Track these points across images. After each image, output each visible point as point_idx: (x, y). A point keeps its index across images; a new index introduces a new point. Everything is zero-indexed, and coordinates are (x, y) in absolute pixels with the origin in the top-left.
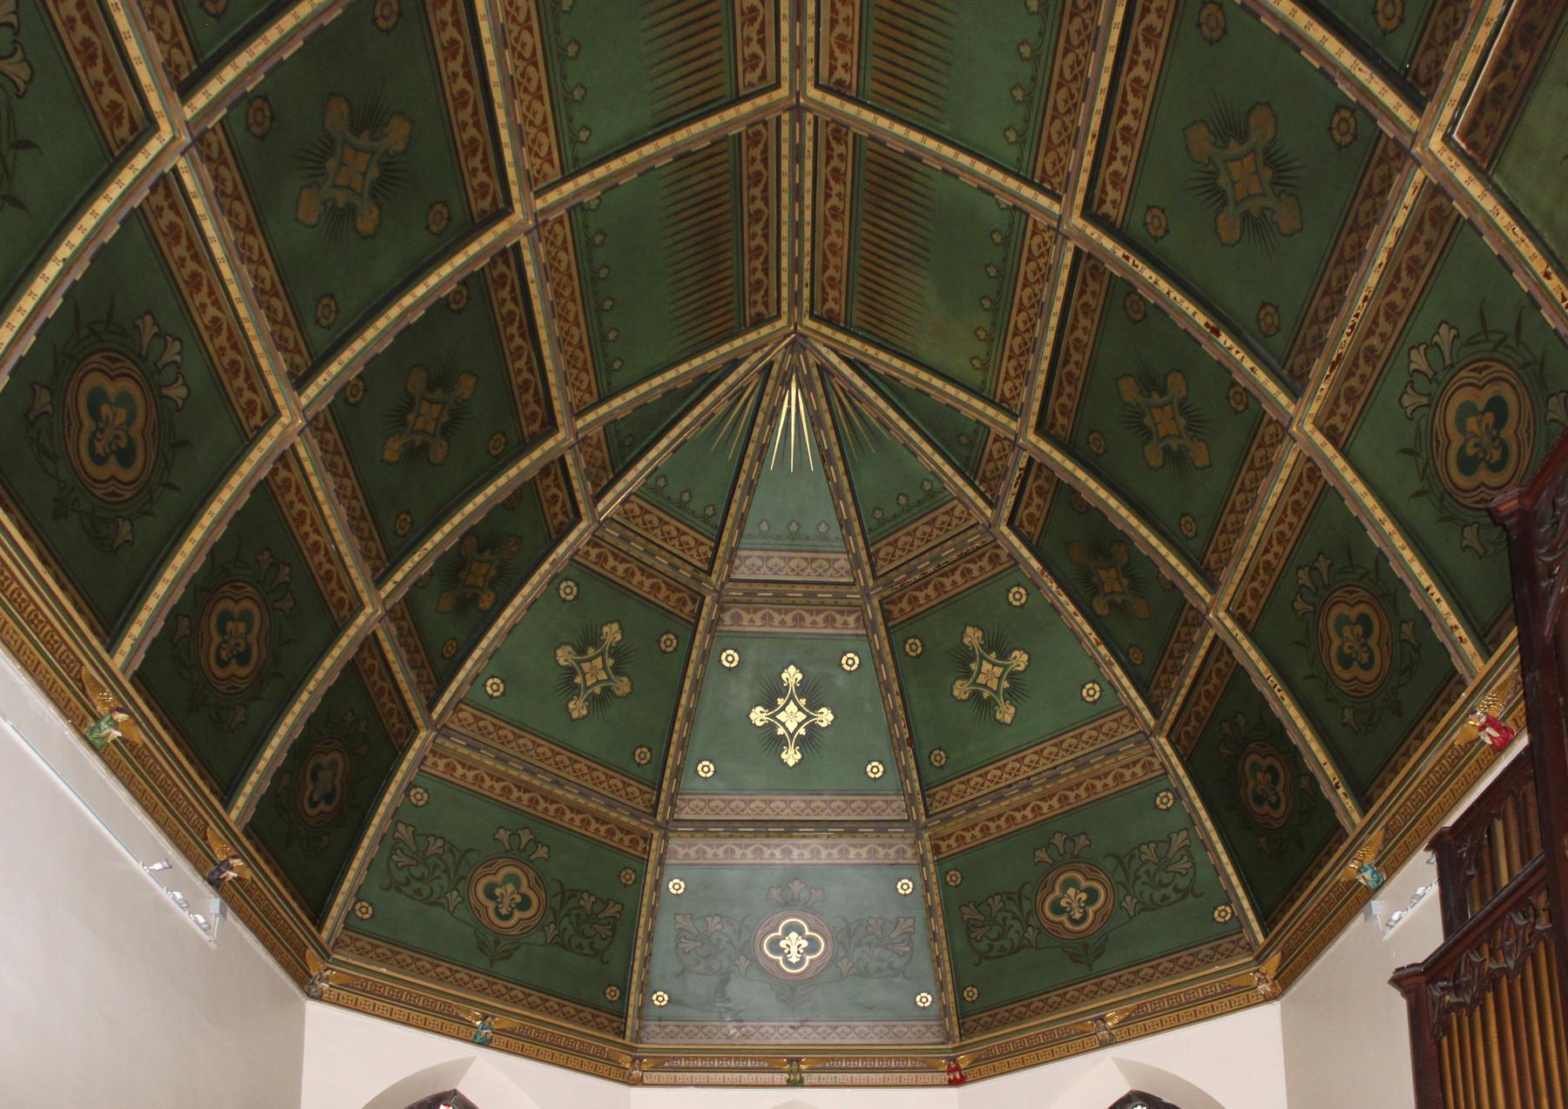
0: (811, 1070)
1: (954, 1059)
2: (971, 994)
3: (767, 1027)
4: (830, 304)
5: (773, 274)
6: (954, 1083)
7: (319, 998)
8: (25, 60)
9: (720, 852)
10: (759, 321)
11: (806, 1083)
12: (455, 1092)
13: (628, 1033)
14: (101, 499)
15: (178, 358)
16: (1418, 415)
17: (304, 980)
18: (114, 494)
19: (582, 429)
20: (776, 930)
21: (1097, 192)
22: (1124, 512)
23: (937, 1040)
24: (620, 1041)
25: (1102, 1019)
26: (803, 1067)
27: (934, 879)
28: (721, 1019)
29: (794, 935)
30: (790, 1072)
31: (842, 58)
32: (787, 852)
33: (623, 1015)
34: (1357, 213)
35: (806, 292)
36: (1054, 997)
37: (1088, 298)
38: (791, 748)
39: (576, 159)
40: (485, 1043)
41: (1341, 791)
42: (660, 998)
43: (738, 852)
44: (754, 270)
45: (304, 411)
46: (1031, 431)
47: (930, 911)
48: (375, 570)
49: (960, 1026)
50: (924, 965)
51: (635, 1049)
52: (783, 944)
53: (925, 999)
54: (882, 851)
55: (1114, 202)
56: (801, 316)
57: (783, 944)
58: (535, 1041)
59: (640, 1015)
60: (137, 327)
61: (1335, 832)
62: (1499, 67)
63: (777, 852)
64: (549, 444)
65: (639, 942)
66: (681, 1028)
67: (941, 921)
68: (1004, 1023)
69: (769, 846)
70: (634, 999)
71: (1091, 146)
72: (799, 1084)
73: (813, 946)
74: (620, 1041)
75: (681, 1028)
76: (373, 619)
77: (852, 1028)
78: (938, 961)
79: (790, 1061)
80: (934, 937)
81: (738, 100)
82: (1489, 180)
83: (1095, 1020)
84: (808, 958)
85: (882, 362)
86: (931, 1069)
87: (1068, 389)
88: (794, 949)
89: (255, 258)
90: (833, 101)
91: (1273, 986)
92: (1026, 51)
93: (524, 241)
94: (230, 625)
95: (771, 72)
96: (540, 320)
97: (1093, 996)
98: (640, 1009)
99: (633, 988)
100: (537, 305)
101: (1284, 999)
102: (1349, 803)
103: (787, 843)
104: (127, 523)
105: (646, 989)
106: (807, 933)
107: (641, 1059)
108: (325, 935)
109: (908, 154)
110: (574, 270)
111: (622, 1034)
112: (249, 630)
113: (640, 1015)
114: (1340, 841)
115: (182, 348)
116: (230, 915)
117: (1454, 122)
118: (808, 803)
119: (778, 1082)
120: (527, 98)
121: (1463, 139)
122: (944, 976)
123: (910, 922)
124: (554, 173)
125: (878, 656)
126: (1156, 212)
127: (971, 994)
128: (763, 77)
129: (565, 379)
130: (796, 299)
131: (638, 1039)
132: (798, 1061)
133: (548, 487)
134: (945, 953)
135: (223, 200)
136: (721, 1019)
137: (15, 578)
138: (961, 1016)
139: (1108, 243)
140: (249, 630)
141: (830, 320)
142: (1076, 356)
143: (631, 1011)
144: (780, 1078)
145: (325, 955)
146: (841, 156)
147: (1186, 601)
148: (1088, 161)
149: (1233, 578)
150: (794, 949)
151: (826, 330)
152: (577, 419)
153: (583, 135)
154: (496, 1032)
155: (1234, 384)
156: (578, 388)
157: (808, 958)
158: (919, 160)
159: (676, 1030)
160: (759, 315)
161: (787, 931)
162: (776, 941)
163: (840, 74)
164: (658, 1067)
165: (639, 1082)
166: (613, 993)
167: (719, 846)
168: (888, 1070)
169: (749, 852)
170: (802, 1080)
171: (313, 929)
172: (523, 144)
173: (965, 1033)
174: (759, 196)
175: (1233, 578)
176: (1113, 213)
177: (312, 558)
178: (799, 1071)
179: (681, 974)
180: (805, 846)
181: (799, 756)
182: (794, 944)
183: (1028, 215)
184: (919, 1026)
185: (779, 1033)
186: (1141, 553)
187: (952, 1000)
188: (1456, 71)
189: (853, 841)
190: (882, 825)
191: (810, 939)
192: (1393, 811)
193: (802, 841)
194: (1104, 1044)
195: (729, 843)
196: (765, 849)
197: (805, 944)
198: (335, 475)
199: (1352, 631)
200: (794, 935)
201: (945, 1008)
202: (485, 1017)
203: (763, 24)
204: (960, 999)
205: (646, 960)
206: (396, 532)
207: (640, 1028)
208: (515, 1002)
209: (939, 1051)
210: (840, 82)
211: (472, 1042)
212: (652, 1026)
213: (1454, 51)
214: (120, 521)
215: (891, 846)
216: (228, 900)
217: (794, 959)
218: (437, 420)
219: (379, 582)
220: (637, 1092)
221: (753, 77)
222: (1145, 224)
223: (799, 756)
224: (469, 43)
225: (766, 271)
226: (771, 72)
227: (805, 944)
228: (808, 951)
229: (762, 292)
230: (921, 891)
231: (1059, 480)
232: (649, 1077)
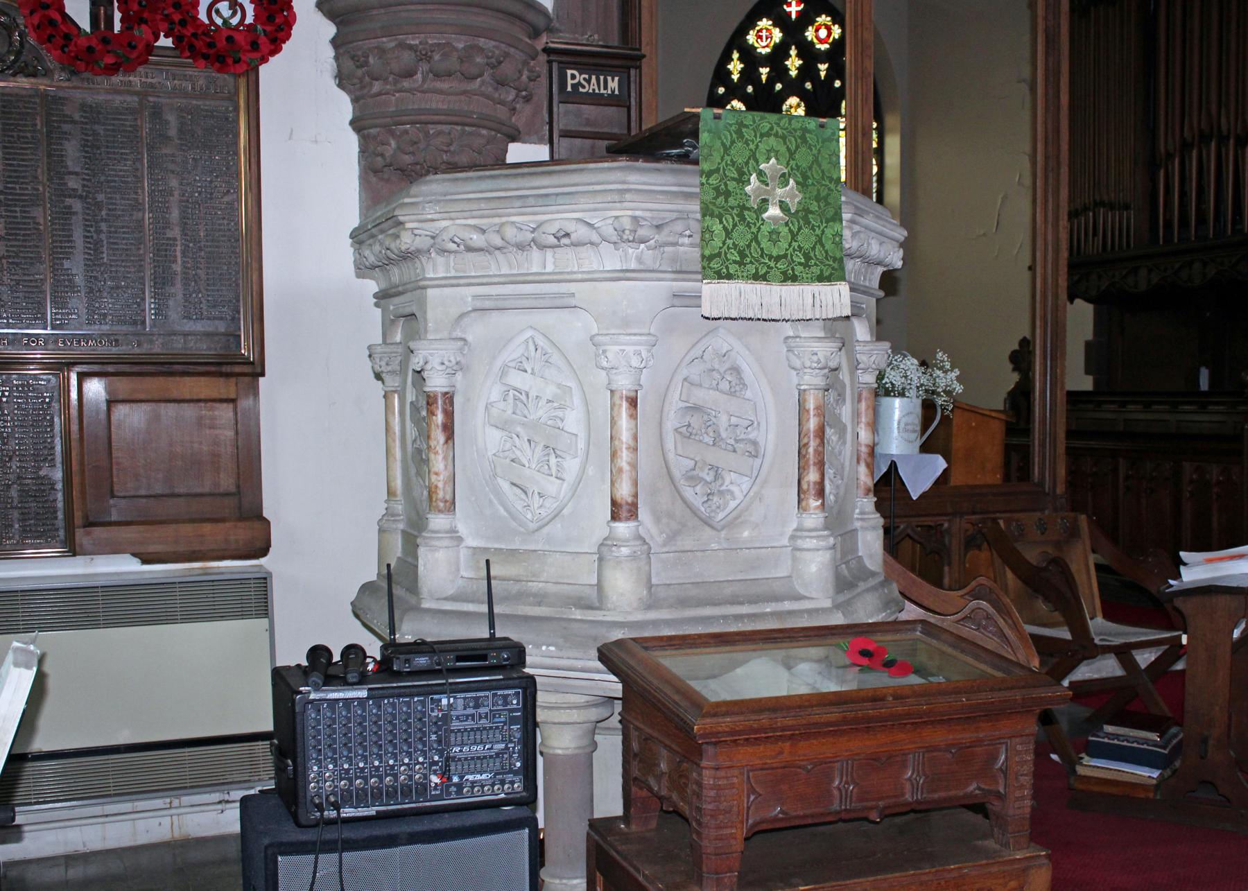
8: (866, 317)
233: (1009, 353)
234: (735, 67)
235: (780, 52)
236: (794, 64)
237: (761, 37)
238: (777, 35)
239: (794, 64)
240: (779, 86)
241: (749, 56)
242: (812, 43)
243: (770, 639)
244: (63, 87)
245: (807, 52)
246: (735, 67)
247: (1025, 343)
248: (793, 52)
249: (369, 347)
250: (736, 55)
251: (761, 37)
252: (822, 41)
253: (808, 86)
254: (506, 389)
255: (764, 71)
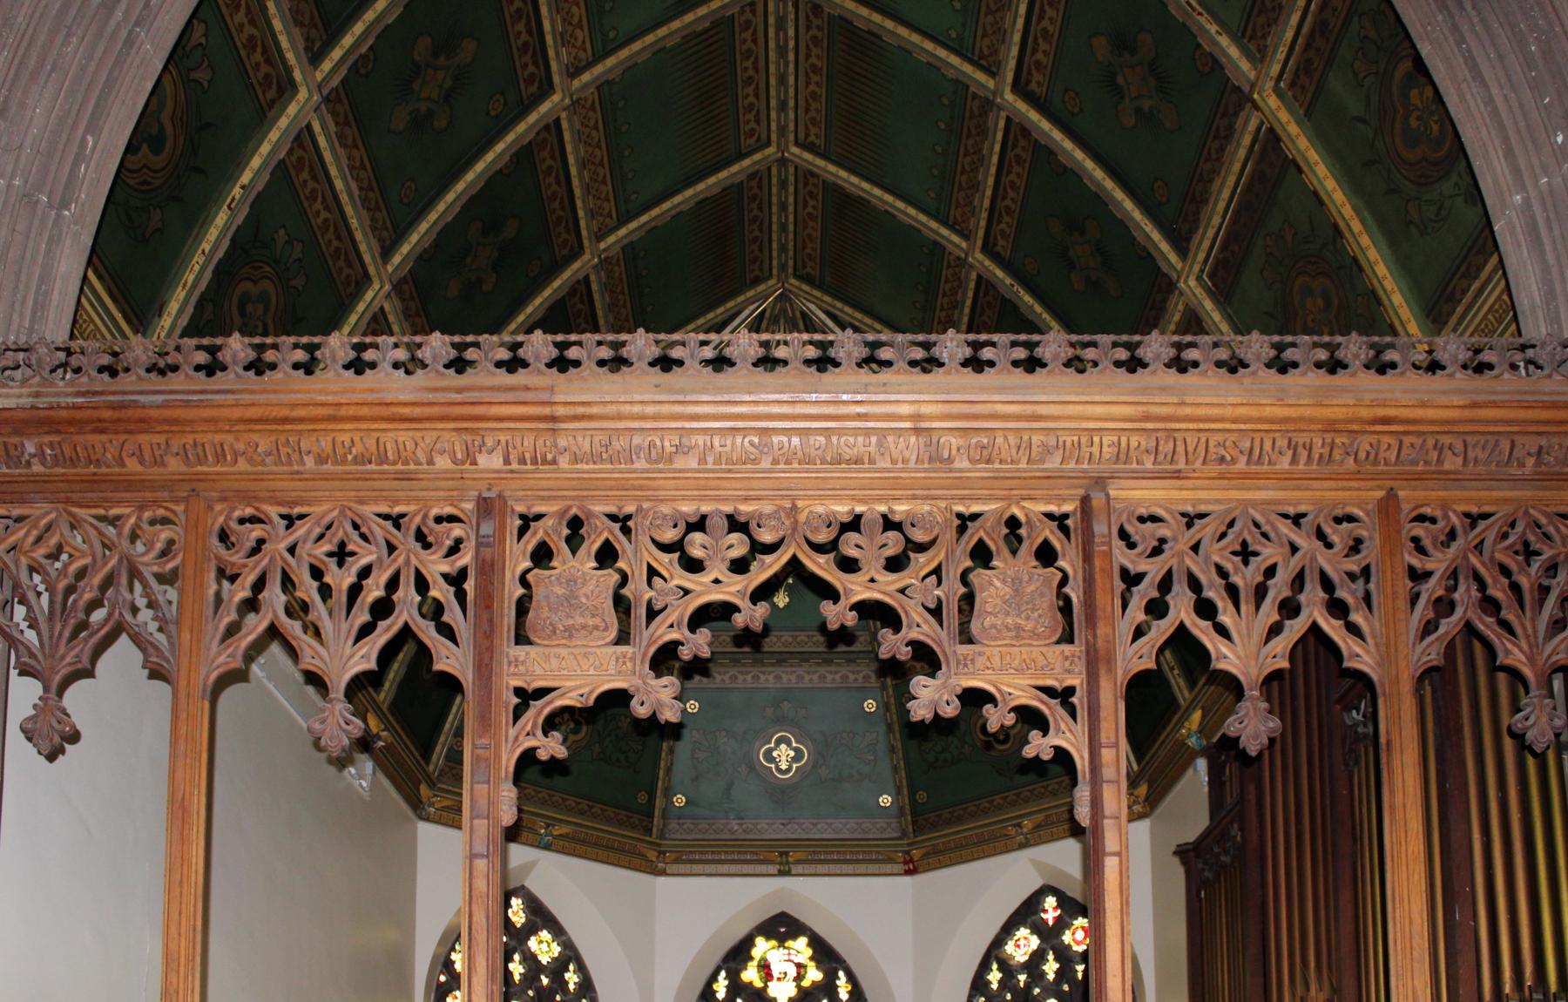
0: (799, 862)
1: (907, 853)
2: (922, 796)
3: (763, 824)
4: (808, 270)
5: (766, 252)
6: (908, 872)
7: (427, 819)
8: (209, 65)
9: (726, 677)
10: (756, 281)
11: (793, 872)
12: (523, 887)
13: (655, 830)
14: (136, 190)
15: (203, 40)
16: (1367, 82)
17: (416, 805)
18: (145, 183)
19: (604, 250)
20: (770, 742)
21: (991, 240)
22: (1099, 174)
23: (895, 835)
24: (648, 838)
25: (1019, 825)
26: (791, 859)
27: (892, 700)
28: (727, 818)
29: (783, 747)
30: (780, 864)
31: (815, 51)
32: (778, 678)
33: (651, 816)
34: (1210, 150)
35: (791, 263)
36: (984, 803)
37: (1045, 23)
38: (782, 592)
39: (628, 212)
40: (547, 847)
41: (1176, 672)
42: (679, 800)
43: (741, 678)
44: (746, 69)
45: (320, 86)
46: (1008, 89)
47: (890, 727)
48: (381, 240)
49: (914, 823)
50: (884, 767)
51: (659, 845)
52: (775, 754)
53: (885, 800)
54: (852, 677)
55: (1037, 83)
56: (787, 277)
57: (775, 754)
58: (583, 842)
59: (664, 816)
60: (273, 239)
61: (1172, 704)
62: (1224, 248)
63: (771, 678)
64: (545, 107)
65: (663, 755)
66: (696, 825)
67: (898, 736)
68: (948, 823)
69: (764, 673)
70: (659, 802)
71: (984, 215)
72: (787, 873)
73: (798, 755)
74: (648, 838)
75: (696, 825)
76: (307, 108)
77: (829, 825)
78: (895, 769)
79: (781, 854)
80: (892, 750)
81: (741, 156)
82: (1225, 309)
83: (1014, 825)
84: (795, 766)
85: (847, 314)
86: (890, 860)
87: (1043, 46)
88: (784, 758)
89: (307, 22)
90: (808, 156)
91: (1144, 807)
92: (939, 149)
93: (564, 115)
94: (250, 308)
95: (764, 136)
96: (600, 313)
97: (1013, 804)
98: (664, 811)
99: (659, 793)
100: (598, 305)
101: (1153, 817)
102: (1182, 682)
103: (778, 670)
104: (158, 211)
105: (669, 793)
106: (794, 745)
107: (664, 853)
108: (431, 768)
109: (870, 32)
110: (624, 276)
111: (649, 831)
112: (266, 310)
113: (664, 816)
114: (1175, 713)
115: (207, 29)
116: (381, 777)
117: (1202, 271)
118: (795, 637)
119: (771, 872)
120: (592, 167)
121: (1210, 279)
122: (901, 781)
123: (874, 735)
124: (611, 223)
125: (887, 706)
126: (1072, 94)
127: (922, 796)
128: (759, 139)
129: (587, 189)
130: (782, 130)
131: (662, 836)
132: (787, 854)
133: (544, 160)
134: (902, 763)
135: (355, 173)
136: (727, 818)
137: (92, 321)
138: (914, 814)
139: (1000, 273)
140: (266, 310)
141: (808, 280)
142: (1011, 194)
143: (657, 812)
144: (773, 869)
145: (432, 785)
146: (816, 110)
147: (1228, 79)
148: (983, 223)
149: (1207, 239)
150: (784, 758)
151: (806, 288)
152: (572, 80)
153: (633, 197)
154: (555, 837)
155: (1199, 46)
156: (574, 46)
157: (795, 766)
158: (879, 37)
159: (692, 827)
160: (757, 277)
161: (778, 742)
162: (770, 751)
163: (812, 138)
164: (677, 861)
165: (663, 873)
166: (643, 798)
167: (725, 673)
168: (857, 861)
169: (749, 678)
170: (790, 870)
171: (422, 763)
172: (589, 193)
173: (918, 830)
174: (750, 39)
175: (1207, 239)
176: (1038, 90)
177: (310, 206)
178: (788, 863)
179: (696, 779)
180: (792, 673)
181: (787, 600)
182: (784, 754)
183: (968, 87)
184: (881, 823)
185: (772, 828)
186: (1177, 20)
187: (907, 801)
188: (1198, 248)
189: (829, 669)
190: (852, 656)
191: (796, 750)
192: (1485, 308)
193: (789, 669)
194: (1022, 846)
195: (733, 671)
196: (761, 676)
197: (792, 753)
198: (369, 209)
199: (1421, 94)
200: (783, 747)
201: (901, 809)
202: (548, 826)
203: (758, 113)
204: (913, 800)
205: (669, 770)
206: (401, 201)
207: (664, 826)
208: (569, 810)
209: (896, 845)
210: (812, 143)
211: (538, 847)
212: (673, 825)
213: (1217, 183)
214: (152, 209)
215: (858, 672)
216: (379, 763)
217: (784, 766)
218: (440, 87)
219: (315, 58)
220: (662, 881)
221: (751, 141)
222: (1064, 102)
223: (787, 600)
224: (555, 141)
225: (758, 121)
226: (764, 136)
227: (792, 753)
228: (795, 759)
229: (751, 31)
230: (882, 710)
231: (1036, 140)
232: (671, 868)
233: (80, 744)
234: (995, 977)
235: (1037, 957)
236: (1051, 967)
237: (1018, 946)
238: (1035, 942)
239: (1051, 967)
240: (1037, 991)
241: (1008, 969)
242: (1069, 946)
243: (94, 408)
244: (107, 80)
245: (1064, 955)
246: (995, 977)
247: (460, 910)
248: (1051, 957)
249: (51, 758)
250: (995, 966)
251: (1018, 946)
252: (1078, 943)
253: (1066, 987)
254: (273, 438)
255: (1022, 978)
